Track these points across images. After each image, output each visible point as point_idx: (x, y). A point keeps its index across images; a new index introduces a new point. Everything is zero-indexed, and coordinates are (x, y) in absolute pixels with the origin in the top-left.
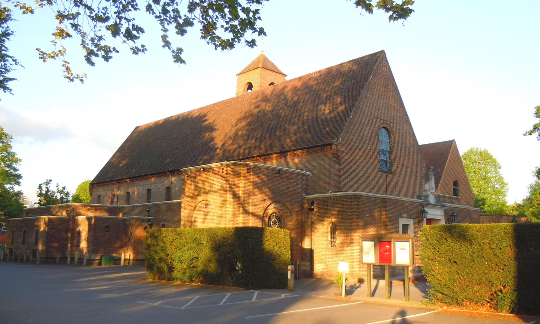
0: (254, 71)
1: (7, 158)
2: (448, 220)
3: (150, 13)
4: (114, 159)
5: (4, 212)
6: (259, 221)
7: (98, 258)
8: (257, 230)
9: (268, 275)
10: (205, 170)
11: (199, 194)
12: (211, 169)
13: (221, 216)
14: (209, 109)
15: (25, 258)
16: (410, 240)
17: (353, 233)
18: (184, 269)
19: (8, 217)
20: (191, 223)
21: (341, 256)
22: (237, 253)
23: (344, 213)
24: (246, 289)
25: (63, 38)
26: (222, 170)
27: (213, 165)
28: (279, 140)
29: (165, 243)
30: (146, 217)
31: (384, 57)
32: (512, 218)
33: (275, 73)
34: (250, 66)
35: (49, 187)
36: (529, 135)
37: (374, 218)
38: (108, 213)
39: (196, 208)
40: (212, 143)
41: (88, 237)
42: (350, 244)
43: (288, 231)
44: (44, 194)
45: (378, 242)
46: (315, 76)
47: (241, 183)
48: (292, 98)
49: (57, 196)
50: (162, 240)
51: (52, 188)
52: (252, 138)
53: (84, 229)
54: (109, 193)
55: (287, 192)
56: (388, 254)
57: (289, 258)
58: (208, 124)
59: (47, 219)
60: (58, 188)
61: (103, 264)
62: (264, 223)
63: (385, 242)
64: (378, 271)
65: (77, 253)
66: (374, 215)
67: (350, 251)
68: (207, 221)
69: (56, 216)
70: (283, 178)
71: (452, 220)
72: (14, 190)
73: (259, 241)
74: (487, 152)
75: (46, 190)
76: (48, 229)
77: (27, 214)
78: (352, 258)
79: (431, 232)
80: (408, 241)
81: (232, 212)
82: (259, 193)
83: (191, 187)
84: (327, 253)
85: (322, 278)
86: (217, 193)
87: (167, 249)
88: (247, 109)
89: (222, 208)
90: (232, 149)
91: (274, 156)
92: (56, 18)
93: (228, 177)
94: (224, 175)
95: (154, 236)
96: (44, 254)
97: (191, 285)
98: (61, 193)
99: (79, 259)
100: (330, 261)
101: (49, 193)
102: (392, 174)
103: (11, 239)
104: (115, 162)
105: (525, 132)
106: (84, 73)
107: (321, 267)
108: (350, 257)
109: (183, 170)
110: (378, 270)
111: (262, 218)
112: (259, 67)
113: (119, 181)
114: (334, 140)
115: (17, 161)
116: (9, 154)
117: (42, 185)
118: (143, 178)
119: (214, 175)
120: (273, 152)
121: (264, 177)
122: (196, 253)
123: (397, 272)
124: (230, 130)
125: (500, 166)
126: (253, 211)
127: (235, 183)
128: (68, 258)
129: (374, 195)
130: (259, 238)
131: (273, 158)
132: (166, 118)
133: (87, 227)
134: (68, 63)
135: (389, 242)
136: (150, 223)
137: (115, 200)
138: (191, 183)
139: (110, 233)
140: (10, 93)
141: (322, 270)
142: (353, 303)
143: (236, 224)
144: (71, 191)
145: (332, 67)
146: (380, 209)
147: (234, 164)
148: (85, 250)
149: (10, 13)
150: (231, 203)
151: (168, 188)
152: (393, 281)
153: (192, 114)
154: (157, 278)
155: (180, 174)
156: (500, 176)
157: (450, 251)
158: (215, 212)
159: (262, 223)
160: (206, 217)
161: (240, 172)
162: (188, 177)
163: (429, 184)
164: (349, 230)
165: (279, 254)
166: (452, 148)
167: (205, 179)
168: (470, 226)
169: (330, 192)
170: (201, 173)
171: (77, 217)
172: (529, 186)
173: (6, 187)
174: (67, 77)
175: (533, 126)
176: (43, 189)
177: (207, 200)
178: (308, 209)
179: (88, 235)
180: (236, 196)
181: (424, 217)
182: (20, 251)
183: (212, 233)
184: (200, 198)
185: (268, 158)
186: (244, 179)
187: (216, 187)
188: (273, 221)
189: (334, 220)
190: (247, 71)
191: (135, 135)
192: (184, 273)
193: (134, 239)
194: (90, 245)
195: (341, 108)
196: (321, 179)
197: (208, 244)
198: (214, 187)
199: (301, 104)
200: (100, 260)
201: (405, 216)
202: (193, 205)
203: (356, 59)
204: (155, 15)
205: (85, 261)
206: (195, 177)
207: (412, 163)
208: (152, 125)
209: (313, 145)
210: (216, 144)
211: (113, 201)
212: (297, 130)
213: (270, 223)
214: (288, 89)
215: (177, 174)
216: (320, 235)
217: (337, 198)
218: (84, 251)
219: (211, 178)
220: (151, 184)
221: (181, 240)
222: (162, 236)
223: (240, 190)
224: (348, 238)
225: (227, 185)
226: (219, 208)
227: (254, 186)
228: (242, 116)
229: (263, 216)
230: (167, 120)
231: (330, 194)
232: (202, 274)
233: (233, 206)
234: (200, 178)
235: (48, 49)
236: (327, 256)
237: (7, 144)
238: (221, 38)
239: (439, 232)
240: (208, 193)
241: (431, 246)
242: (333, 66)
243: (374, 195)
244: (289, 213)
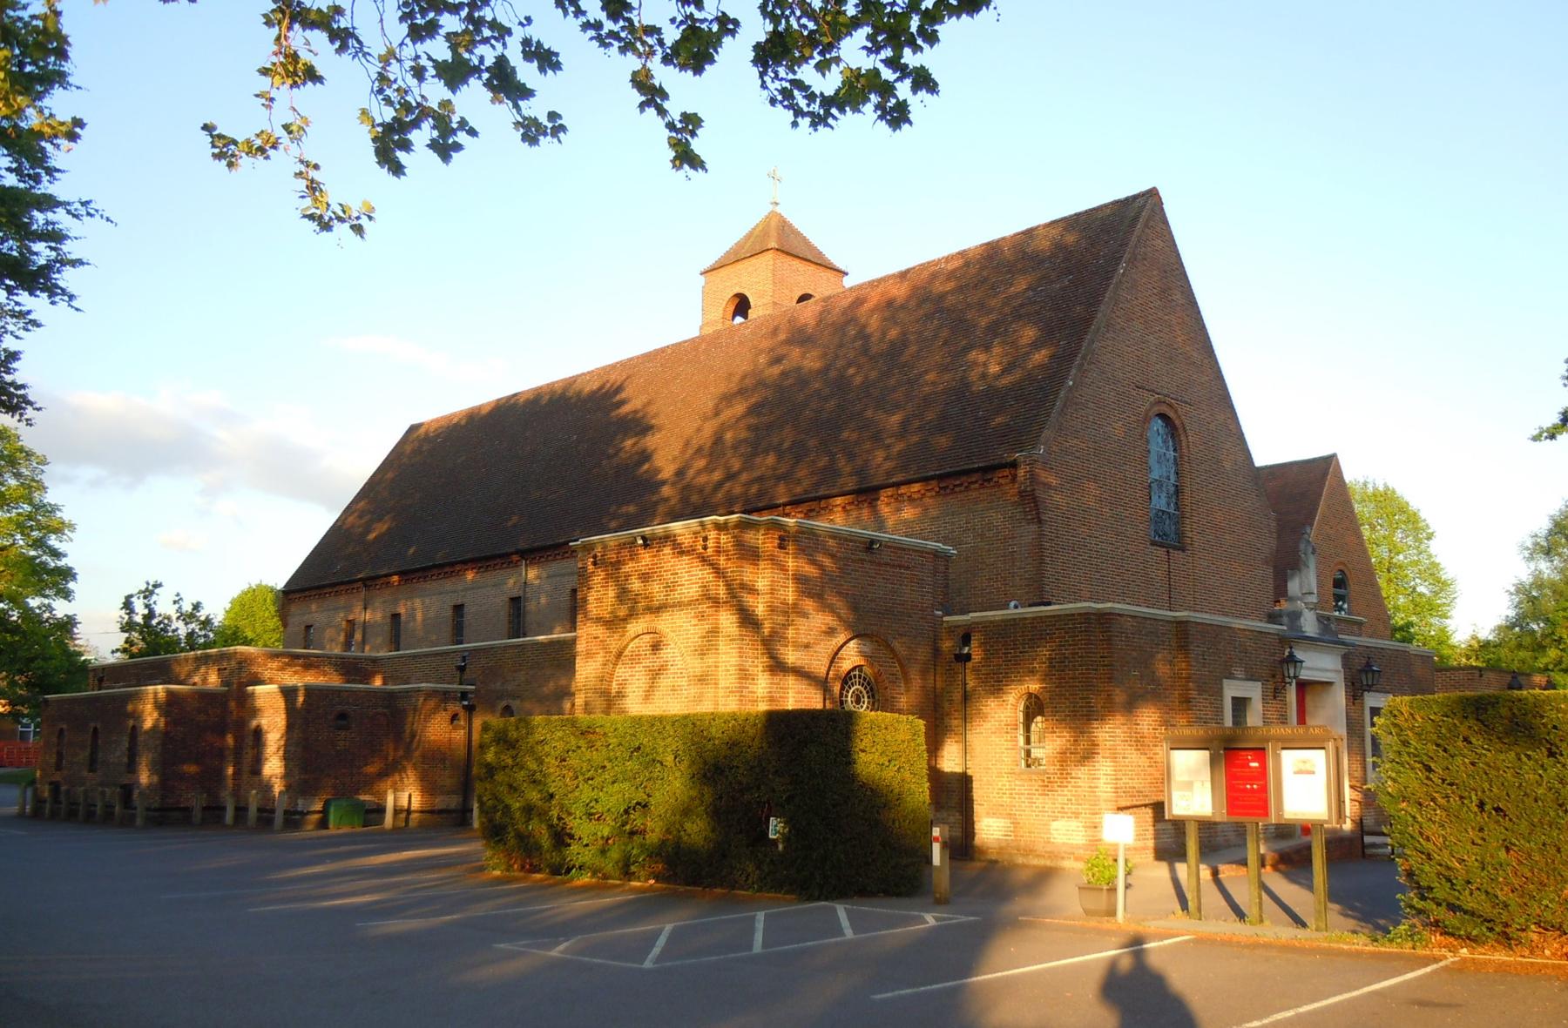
0: (753, 260)
1: (30, 520)
2: (1353, 684)
3: (566, 13)
4: (351, 519)
5: (26, 677)
6: (816, 694)
7: (318, 806)
8: (833, 720)
9: (868, 854)
10: (648, 542)
11: (631, 615)
12: (668, 538)
13: (702, 679)
14: (630, 372)
15: (99, 810)
16: (1331, 745)
17: (1096, 726)
18: (602, 838)
19: (37, 690)
20: (606, 700)
21: (1058, 795)
22: (774, 791)
23: (1065, 666)
24: (804, 898)
25: (295, 85)
26: (702, 542)
27: (677, 527)
28: (851, 456)
29: (541, 762)
30: (455, 686)
31: (1156, 208)
32: (1509, 678)
33: (812, 268)
34: (739, 245)
35: (155, 603)
36: (1548, 440)
37: (1153, 680)
38: (342, 675)
39: (622, 658)
40: (646, 467)
41: (286, 745)
42: (1088, 758)
43: (921, 721)
44: (138, 624)
45: (1222, 752)
46: (950, 267)
47: (760, 580)
48: (884, 334)
49: (177, 629)
50: (532, 751)
51: (164, 606)
52: (766, 452)
53: (273, 722)
54: (339, 619)
55: (891, 607)
56: (1255, 786)
57: (924, 803)
58: (627, 414)
59: (162, 695)
60: (180, 608)
61: (331, 826)
62: (829, 699)
63: (1243, 753)
64: (1168, 838)
65: (254, 792)
66: (1154, 672)
67: (1088, 779)
68: (657, 693)
69: (188, 685)
70: (879, 564)
71: (1365, 683)
72: (54, 612)
73: (840, 752)
74: (1394, 492)
75: (146, 612)
76: (167, 724)
77: (101, 680)
78: (1095, 801)
79: (1417, 717)
80: (1323, 748)
81: (735, 666)
82: (814, 610)
83: (605, 594)
84: (1015, 785)
85: (1000, 860)
86: (687, 609)
87: (548, 780)
88: (745, 367)
89: (705, 654)
90: (707, 483)
91: (838, 502)
92: (266, 23)
93: (722, 561)
94: (708, 556)
95: (506, 742)
96: (157, 798)
97: (627, 888)
98: (188, 620)
99: (259, 810)
100: (1024, 811)
101: (154, 622)
102: (1183, 551)
103: (54, 756)
104: (353, 526)
105: (1537, 432)
106: (365, 203)
107: (998, 827)
108: (1090, 796)
109: (579, 543)
110: (1165, 834)
111: (823, 684)
112: (768, 250)
113: (369, 582)
114: (1021, 451)
115: (60, 529)
116: (40, 508)
117: (133, 599)
118: (440, 574)
119: (678, 557)
120: (835, 491)
121: (827, 562)
122: (640, 789)
123: (1220, 839)
124: (699, 430)
125: (1430, 531)
126: (799, 663)
127: (743, 580)
128: (228, 808)
129: (1152, 611)
130: (839, 742)
131: (835, 509)
132: (498, 400)
133: (284, 716)
134: (316, 167)
135: (1260, 753)
136: (466, 703)
137: (358, 636)
138: (606, 582)
139: (351, 733)
140: (69, 305)
141: (1001, 837)
142: (1166, 942)
143: (749, 701)
144: (216, 615)
145: (998, 241)
146: (1171, 653)
147: (743, 526)
148: (276, 786)
149: (63, 66)
150: (734, 640)
151: (516, 601)
152: (1221, 867)
153: (577, 386)
154: (516, 866)
155: (550, 558)
156: (1432, 560)
157: (1484, 776)
158: (683, 667)
159: (824, 695)
160: (653, 683)
161: (758, 548)
162: (595, 563)
163: (1301, 578)
164: (1082, 716)
165: (896, 791)
166: (1329, 477)
167: (650, 569)
168: (1548, 697)
169: (1012, 604)
170: (638, 550)
171: (250, 688)
172: (1514, 588)
173: (31, 606)
174: (311, 217)
175: (1559, 413)
176: (137, 611)
177: (655, 633)
178: (953, 656)
179: (287, 740)
180: (747, 619)
181: (1292, 675)
182: (82, 788)
183: (692, 728)
184: (635, 627)
185: (817, 509)
186: (773, 568)
187: (684, 593)
188: (853, 692)
189: (1037, 686)
190: (734, 262)
191: (408, 448)
192: (603, 852)
193: (421, 749)
194: (291, 770)
195: (1040, 356)
196: (984, 567)
197: (680, 763)
198: (679, 594)
199: (913, 348)
200: (325, 812)
201: (1239, 672)
202: (614, 645)
203: (1071, 216)
204: (583, 19)
205: (279, 818)
206: (617, 564)
207: (1238, 521)
208: (461, 419)
209: (958, 469)
210: (658, 471)
211: (350, 642)
212: (904, 424)
213: (844, 699)
214: (867, 306)
215: (543, 559)
216: (992, 733)
217: (1042, 622)
218: (272, 786)
219: (667, 566)
220: (462, 591)
221: (591, 752)
222: (531, 740)
223: (760, 601)
224: (1081, 741)
225: (719, 586)
226: (695, 655)
227: (798, 587)
228: (733, 386)
229: (827, 678)
230: (504, 404)
231: (1013, 611)
232: (658, 854)
233: (740, 648)
234: (634, 567)
235: (241, 125)
236: (1016, 794)
237: (33, 480)
238: (810, 87)
239: (1445, 719)
240: (658, 612)
241: (1415, 761)
242: (1003, 239)
243: (1152, 611)
244: (898, 669)
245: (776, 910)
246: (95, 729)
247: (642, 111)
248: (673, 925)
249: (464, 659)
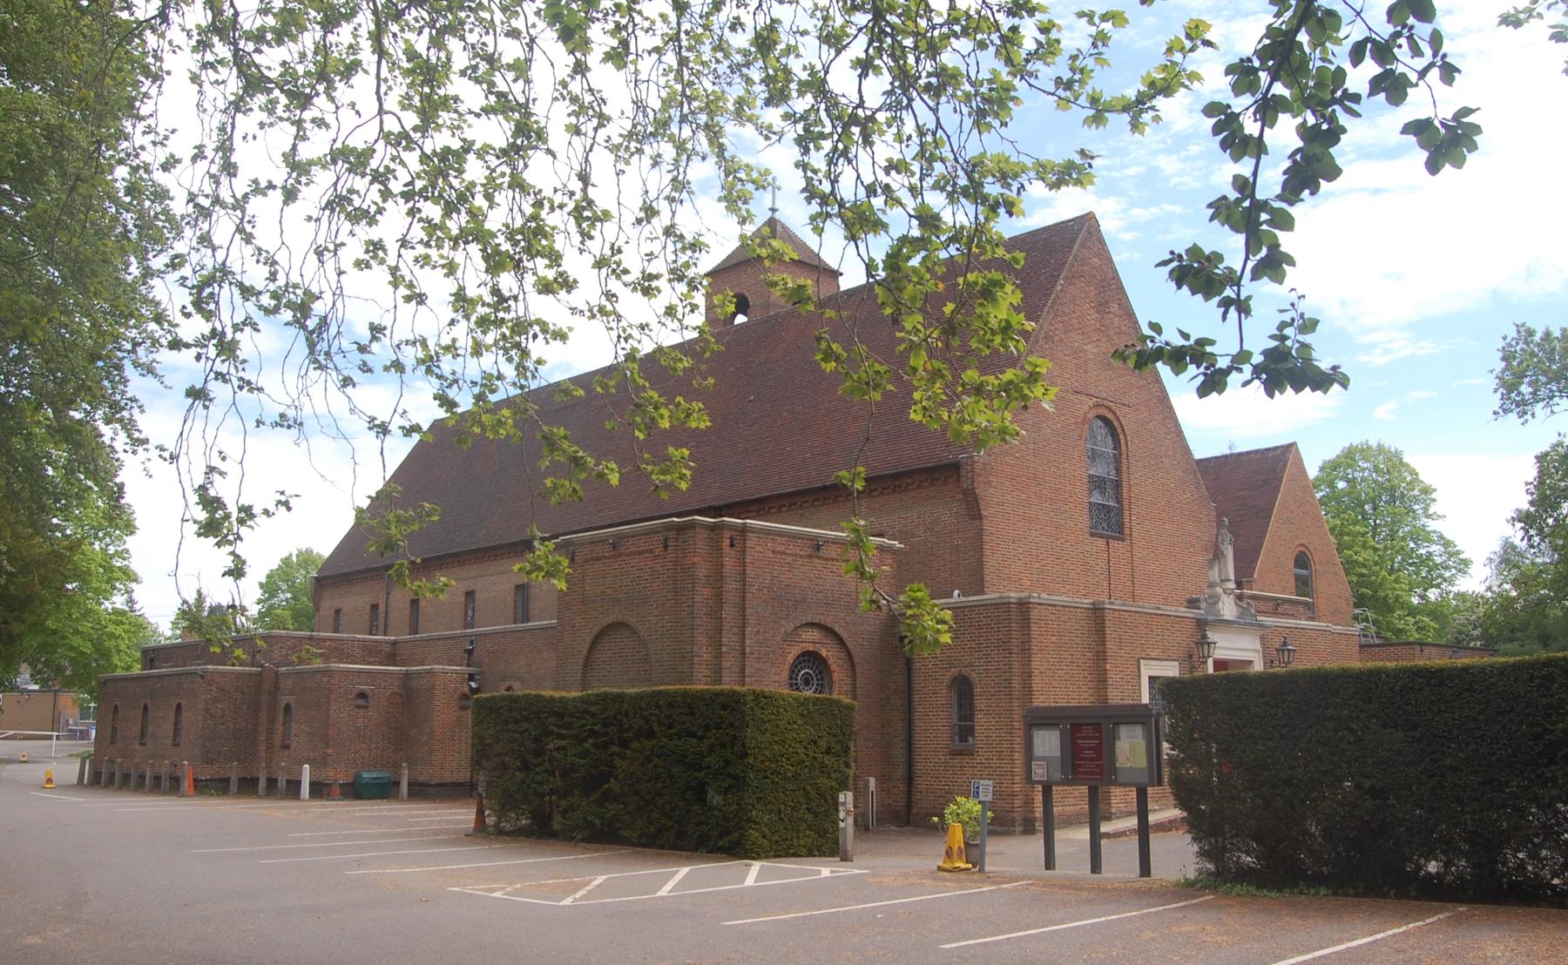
70: (826, 559)
246: (146, 707)
247: (199, 593)
248: (658, 894)
249: (472, 643)
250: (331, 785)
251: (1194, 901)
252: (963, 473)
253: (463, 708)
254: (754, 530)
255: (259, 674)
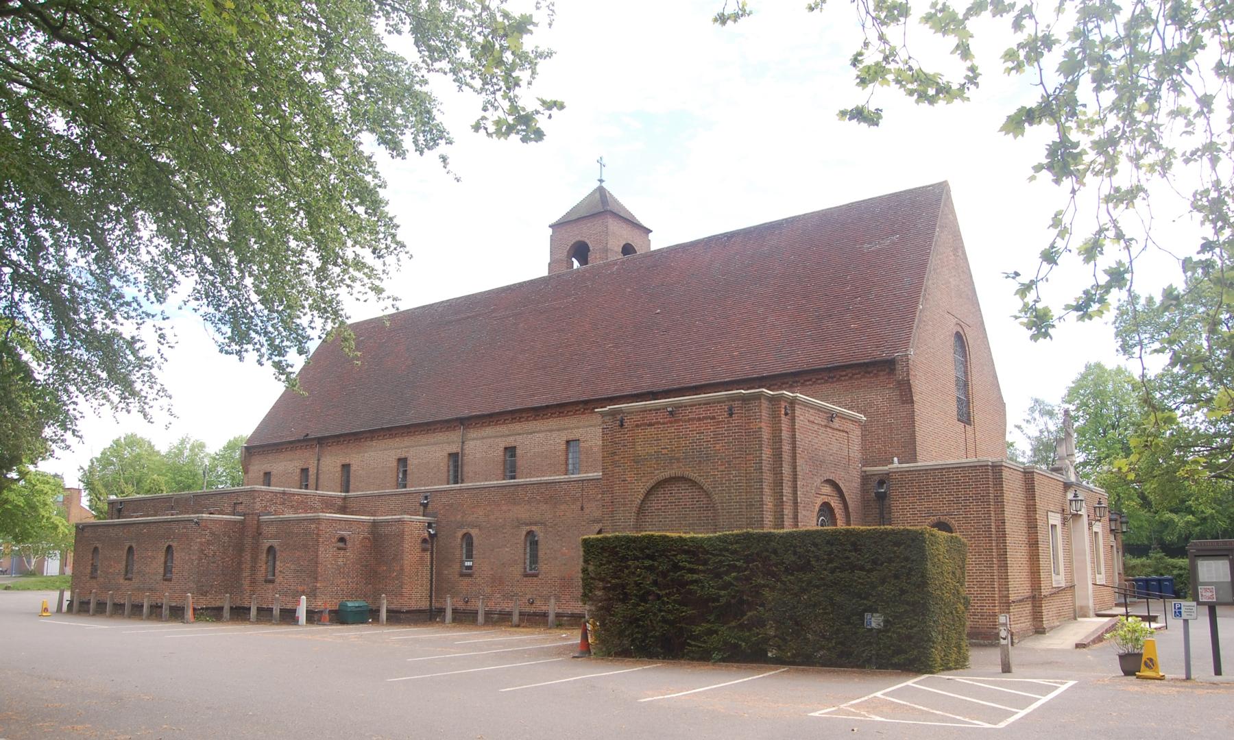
70: (833, 429)
245: (741, 681)
246: (130, 548)
250: (321, 612)
251: (765, 675)
252: (899, 367)
253: (424, 550)
254: (806, 405)
255: (241, 522)
